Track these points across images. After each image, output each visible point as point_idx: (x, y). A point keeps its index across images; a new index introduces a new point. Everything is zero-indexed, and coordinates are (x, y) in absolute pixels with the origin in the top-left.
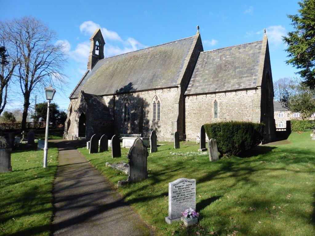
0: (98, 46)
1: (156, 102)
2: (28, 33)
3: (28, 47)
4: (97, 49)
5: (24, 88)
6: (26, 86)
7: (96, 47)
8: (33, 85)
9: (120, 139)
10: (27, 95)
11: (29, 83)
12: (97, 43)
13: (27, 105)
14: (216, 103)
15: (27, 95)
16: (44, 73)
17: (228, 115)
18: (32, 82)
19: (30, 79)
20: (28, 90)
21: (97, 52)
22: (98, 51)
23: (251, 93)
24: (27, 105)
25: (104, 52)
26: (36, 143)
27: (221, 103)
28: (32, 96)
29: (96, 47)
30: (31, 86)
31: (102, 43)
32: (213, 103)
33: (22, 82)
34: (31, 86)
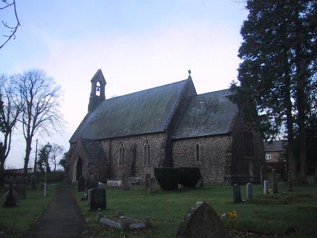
0: (99, 87)
1: (147, 146)
2: (30, 83)
3: (31, 93)
4: (98, 90)
5: (26, 133)
6: (28, 131)
7: (97, 88)
8: (35, 130)
9: (64, 170)
10: (29, 140)
11: (31, 129)
12: (98, 84)
13: (29, 149)
14: (198, 146)
15: (29, 140)
16: (44, 118)
17: (208, 159)
18: (34, 128)
19: (31, 124)
20: (30, 134)
21: (98, 93)
22: (99, 92)
23: (225, 138)
24: (29, 149)
25: (105, 93)
26: (198, 95)
27: (202, 147)
28: (34, 139)
29: (97, 88)
30: (32, 132)
31: (103, 83)
32: (195, 147)
33: (25, 127)
34: (32, 132)
